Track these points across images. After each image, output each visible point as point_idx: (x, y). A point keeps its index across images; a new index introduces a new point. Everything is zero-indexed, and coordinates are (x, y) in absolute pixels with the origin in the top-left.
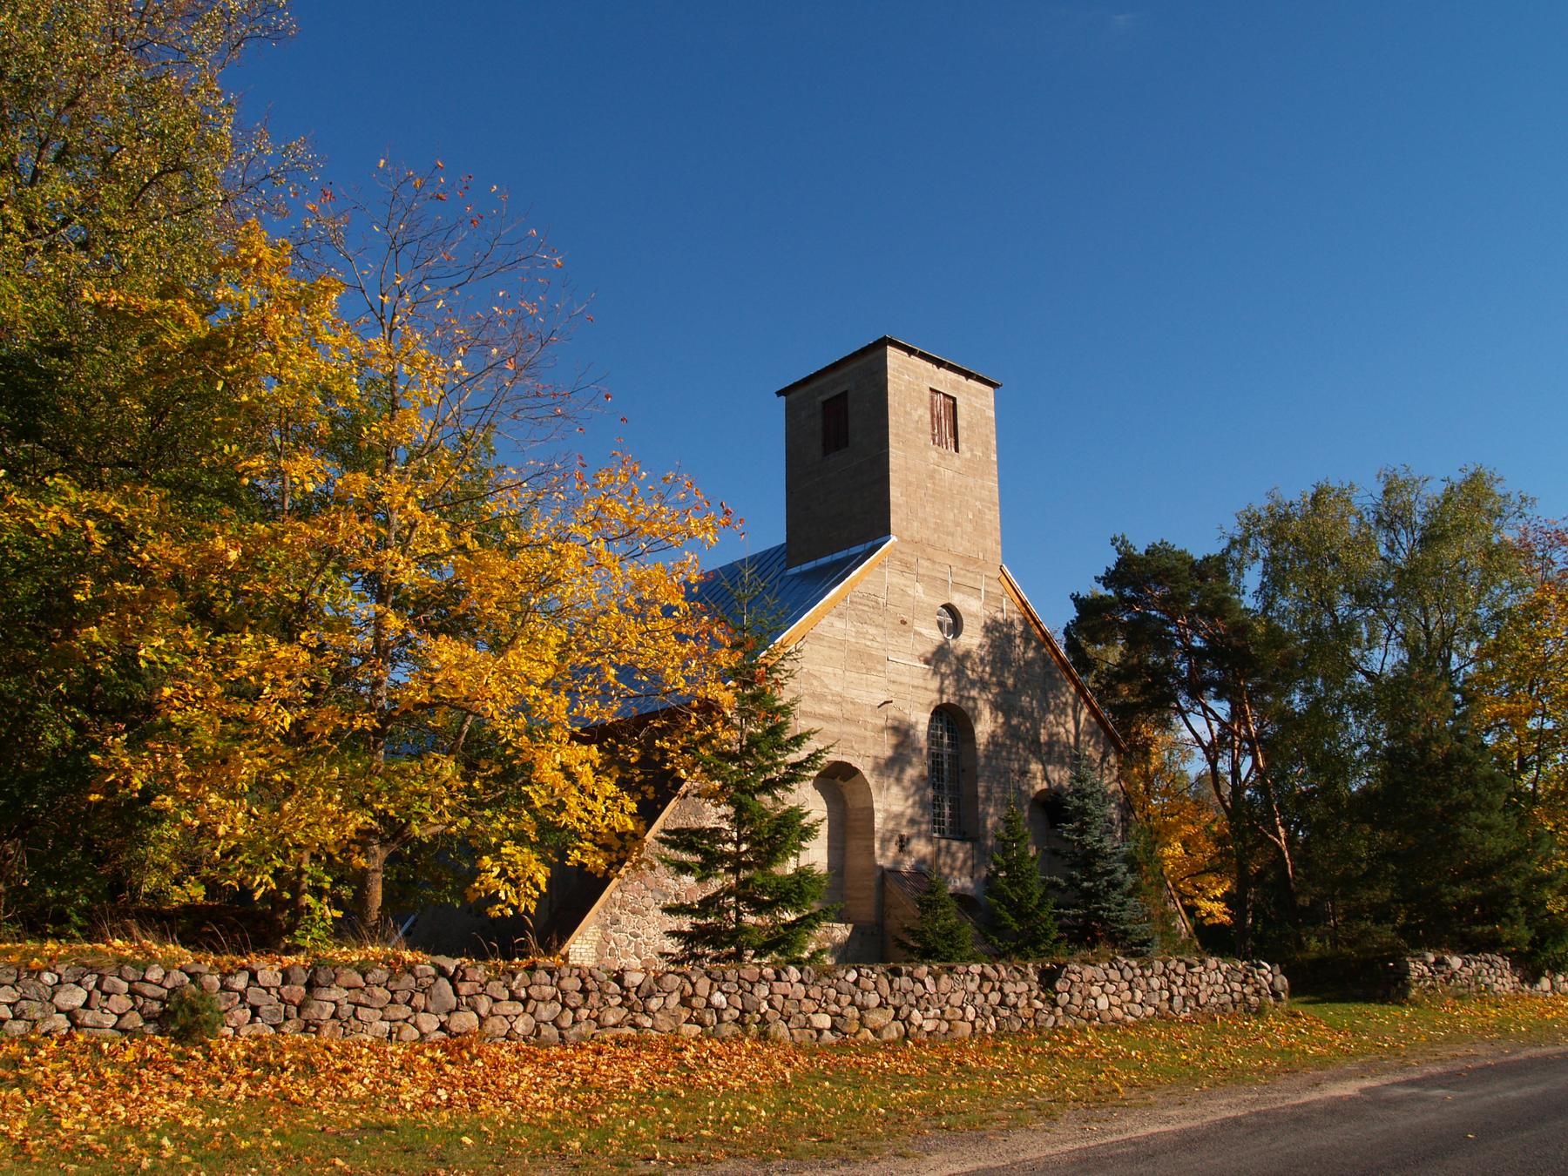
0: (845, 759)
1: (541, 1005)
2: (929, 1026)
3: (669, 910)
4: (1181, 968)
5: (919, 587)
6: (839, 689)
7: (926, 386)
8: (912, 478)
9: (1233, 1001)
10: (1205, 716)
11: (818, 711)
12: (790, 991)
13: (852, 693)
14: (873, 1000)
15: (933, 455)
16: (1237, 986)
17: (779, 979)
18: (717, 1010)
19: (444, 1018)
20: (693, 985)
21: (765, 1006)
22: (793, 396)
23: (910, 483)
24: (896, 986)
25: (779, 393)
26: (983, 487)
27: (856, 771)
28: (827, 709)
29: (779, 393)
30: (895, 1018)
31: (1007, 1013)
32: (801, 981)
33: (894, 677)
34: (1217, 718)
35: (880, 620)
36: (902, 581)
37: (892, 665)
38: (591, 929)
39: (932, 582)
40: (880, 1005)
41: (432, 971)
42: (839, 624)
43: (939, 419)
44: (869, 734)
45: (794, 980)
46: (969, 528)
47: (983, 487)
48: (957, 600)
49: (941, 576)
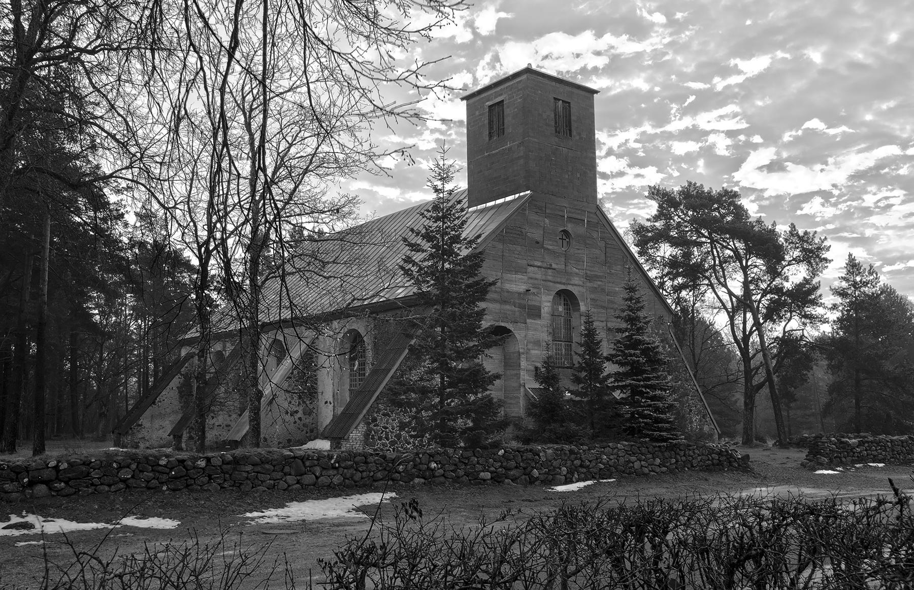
9: (713, 464)
22: (472, 101)
27: (509, 331)
33: (531, 275)
38: (361, 425)
48: (569, 227)
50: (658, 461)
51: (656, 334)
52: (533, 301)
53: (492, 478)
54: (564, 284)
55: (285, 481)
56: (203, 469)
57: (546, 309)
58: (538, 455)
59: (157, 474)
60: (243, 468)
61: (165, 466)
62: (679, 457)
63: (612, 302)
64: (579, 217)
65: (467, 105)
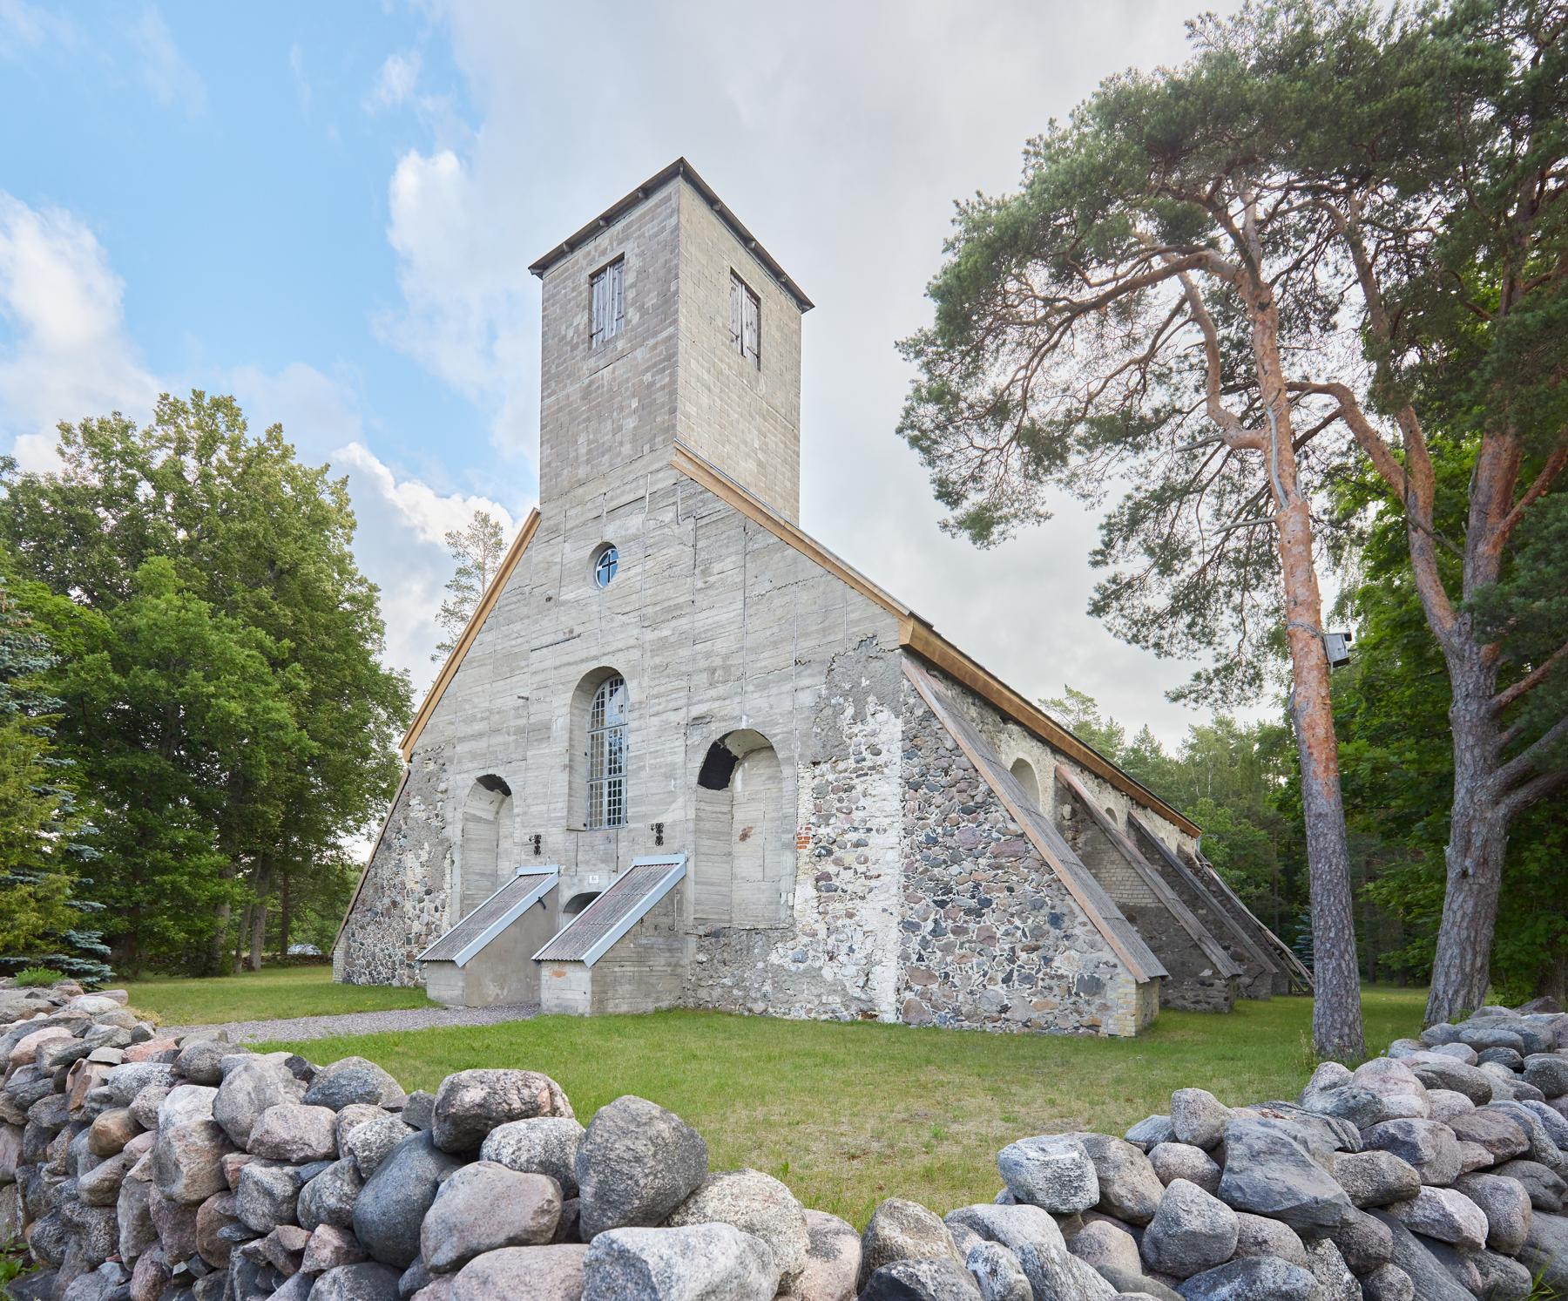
6: (487, 704)
28: (479, 727)
52: (538, 713)
54: (596, 658)
57: (486, 1018)
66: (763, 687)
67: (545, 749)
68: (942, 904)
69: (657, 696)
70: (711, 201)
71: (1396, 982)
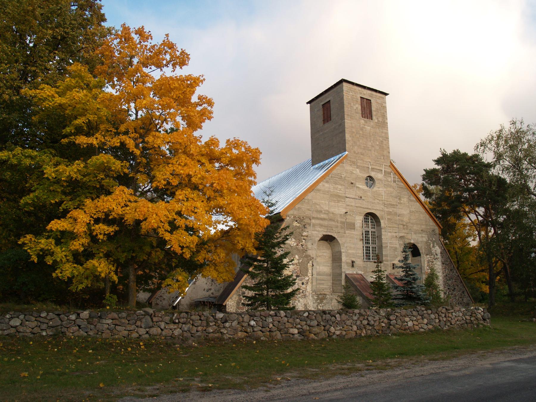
0: (330, 234)
1: (184, 325)
2: (338, 333)
3: (298, 289)
4: (444, 310)
5: (358, 170)
6: (327, 209)
7: (359, 96)
8: (354, 130)
9: (466, 323)
10: (475, 214)
11: (319, 216)
12: (281, 320)
13: (332, 210)
14: (315, 323)
15: (362, 121)
16: (468, 317)
17: (276, 315)
18: (252, 326)
19: (147, 330)
20: (243, 318)
21: (271, 325)
22: (313, 103)
23: (354, 132)
24: (324, 318)
25: (307, 103)
26: (382, 132)
27: (334, 238)
28: (323, 216)
29: (307, 103)
30: (324, 330)
31: (370, 328)
32: (286, 316)
33: (348, 203)
34: (480, 215)
35: (343, 183)
36: (351, 168)
37: (347, 199)
38: (235, 296)
39: (363, 169)
40: (318, 325)
41: (143, 313)
42: (327, 185)
43: (364, 108)
44: (339, 224)
45: (282, 316)
46: (377, 148)
47: (382, 132)
48: (373, 174)
49: (367, 166)
50: (425, 321)
51: (431, 241)
52: (349, 219)
53: (299, 333)
54: (370, 209)
55: (137, 332)
56: (74, 321)
57: (358, 225)
58: (335, 317)
59: (39, 324)
60: (104, 321)
61: (45, 318)
62: (441, 318)
63: (402, 221)
64: (379, 168)
65: (310, 106)
66: (415, 233)
67: (353, 232)
68: (449, 289)
69: (390, 227)
70: (353, 83)
71: (384, 105)
